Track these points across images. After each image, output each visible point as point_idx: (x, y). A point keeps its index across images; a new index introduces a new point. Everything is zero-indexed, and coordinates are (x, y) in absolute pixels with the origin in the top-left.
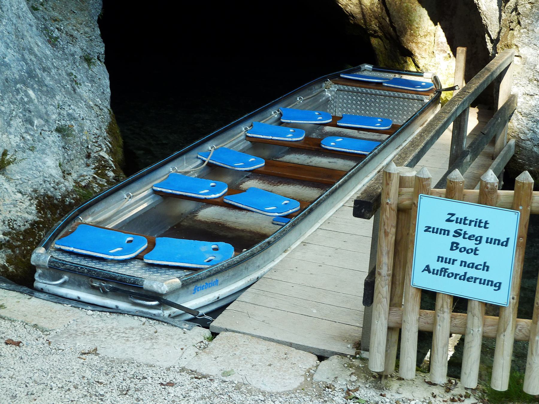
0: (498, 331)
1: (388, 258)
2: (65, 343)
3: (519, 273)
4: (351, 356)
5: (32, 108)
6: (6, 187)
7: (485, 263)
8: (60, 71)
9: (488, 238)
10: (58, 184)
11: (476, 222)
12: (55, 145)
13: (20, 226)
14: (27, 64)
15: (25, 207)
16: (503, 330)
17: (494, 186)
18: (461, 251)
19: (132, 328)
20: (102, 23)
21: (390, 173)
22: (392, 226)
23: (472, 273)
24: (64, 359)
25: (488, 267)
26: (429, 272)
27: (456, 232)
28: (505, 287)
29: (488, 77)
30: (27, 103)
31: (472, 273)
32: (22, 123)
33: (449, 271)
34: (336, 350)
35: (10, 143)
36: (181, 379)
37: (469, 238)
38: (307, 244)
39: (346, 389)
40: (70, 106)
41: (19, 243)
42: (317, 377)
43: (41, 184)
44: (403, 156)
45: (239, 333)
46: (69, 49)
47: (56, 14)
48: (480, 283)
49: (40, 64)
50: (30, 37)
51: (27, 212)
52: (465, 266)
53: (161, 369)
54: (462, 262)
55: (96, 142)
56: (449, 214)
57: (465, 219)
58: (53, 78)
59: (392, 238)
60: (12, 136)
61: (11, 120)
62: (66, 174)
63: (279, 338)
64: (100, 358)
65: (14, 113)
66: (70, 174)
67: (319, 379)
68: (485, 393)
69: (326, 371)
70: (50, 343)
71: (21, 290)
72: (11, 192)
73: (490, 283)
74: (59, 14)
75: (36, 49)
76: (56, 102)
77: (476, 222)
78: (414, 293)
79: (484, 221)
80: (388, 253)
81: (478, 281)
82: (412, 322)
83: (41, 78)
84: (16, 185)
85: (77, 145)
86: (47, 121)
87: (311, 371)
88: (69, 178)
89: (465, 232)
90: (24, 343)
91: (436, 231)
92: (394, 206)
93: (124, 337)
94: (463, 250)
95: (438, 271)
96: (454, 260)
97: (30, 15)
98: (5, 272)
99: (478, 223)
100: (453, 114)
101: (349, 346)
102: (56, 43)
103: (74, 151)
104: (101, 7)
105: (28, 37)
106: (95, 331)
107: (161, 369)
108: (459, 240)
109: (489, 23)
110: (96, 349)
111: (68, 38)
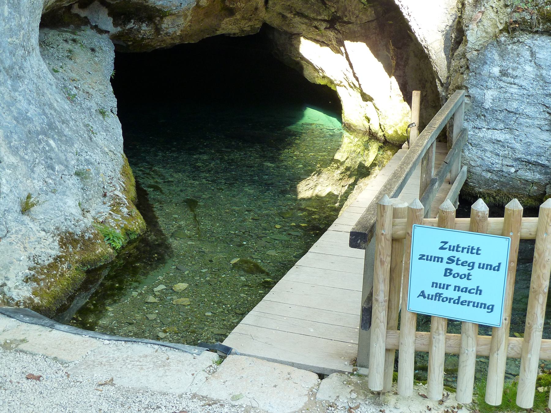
0: (491, 349)
1: (385, 285)
2: (83, 375)
3: (511, 295)
4: (349, 373)
5: (53, 156)
6: (31, 226)
7: (478, 287)
8: (78, 123)
9: (480, 264)
10: (78, 221)
11: (468, 249)
12: (75, 187)
13: (44, 261)
14: (47, 117)
15: (48, 243)
16: (496, 349)
17: (484, 214)
18: (454, 277)
19: (146, 356)
20: (113, 81)
21: (384, 206)
22: (387, 255)
23: (465, 296)
24: (82, 392)
25: (481, 291)
26: (425, 297)
27: (449, 259)
28: (497, 309)
29: (448, 114)
30: (48, 151)
31: (465, 296)
32: (44, 169)
33: (443, 296)
34: (335, 368)
35: (34, 187)
36: (192, 406)
37: (462, 264)
38: (300, 267)
39: (348, 407)
40: (87, 152)
41: (43, 276)
42: (319, 396)
43: (62, 222)
44: (389, 187)
45: (245, 355)
46: (86, 104)
47: (74, 75)
48: (474, 306)
49: (60, 117)
50: (51, 94)
51: (50, 248)
52: (458, 291)
53: (174, 396)
54: (455, 287)
55: (111, 183)
56: (442, 242)
57: (458, 246)
58: (71, 129)
59: (387, 266)
60: (36, 181)
61: (34, 166)
62: (85, 212)
63: (282, 359)
64: (116, 388)
65: (37, 160)
66: (89, 211)
67: (322, 398)
68: (475, 403)
69: (329, 389)
70: (68, 376)
71: (43, 323)
72: (36, 231)
73: (483, 305)
74: (77, 75)
75: (55, 105)
76: (75, 150)
77: (468, 249)
78: (410, 317)
79: (476, 248)
80: (384, 280)
81: (471, 304)
82: (410, 342)
83: (61, 129)
84: (40, 225)
85: (94, 186)
86: (67, 167)
87: (314, 390)
88: (88, 215)
89: (458, 259)
90: (44, 376)
91: (429, 259)
92: (389, 237)
93: (138, 365)
94: (456, 275)
95: (432, 296)
96: (448, 286)
97: (50, 76)
98: (32, 303)
99: (471, 250)
100: (425, 147)
101: (346, 363)
102: (74, 99)
103: (92, 192)
104: (113, 68)
105: (48, 94)
106: (111, 361)
107: (174, 396)
108: (453, 266)
109: (439, 69)
110: (112, 380)
111: (84, 94)
